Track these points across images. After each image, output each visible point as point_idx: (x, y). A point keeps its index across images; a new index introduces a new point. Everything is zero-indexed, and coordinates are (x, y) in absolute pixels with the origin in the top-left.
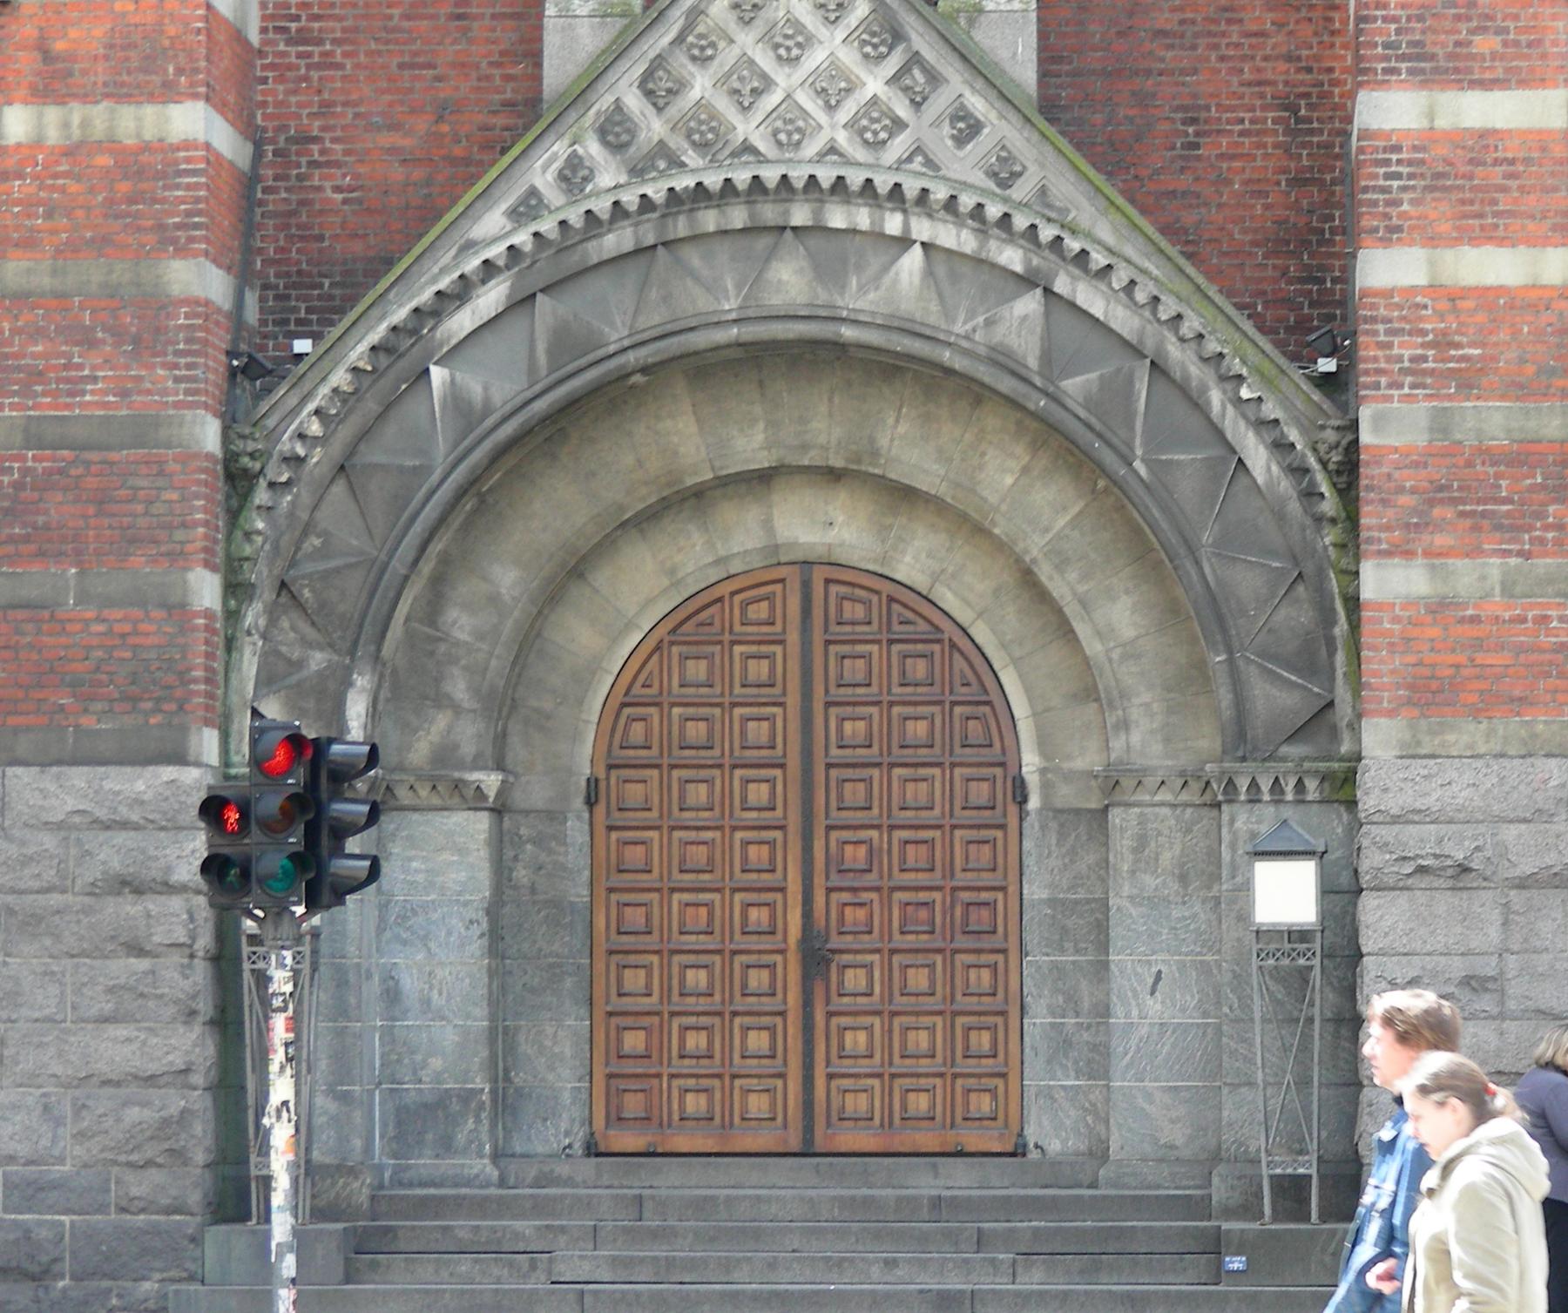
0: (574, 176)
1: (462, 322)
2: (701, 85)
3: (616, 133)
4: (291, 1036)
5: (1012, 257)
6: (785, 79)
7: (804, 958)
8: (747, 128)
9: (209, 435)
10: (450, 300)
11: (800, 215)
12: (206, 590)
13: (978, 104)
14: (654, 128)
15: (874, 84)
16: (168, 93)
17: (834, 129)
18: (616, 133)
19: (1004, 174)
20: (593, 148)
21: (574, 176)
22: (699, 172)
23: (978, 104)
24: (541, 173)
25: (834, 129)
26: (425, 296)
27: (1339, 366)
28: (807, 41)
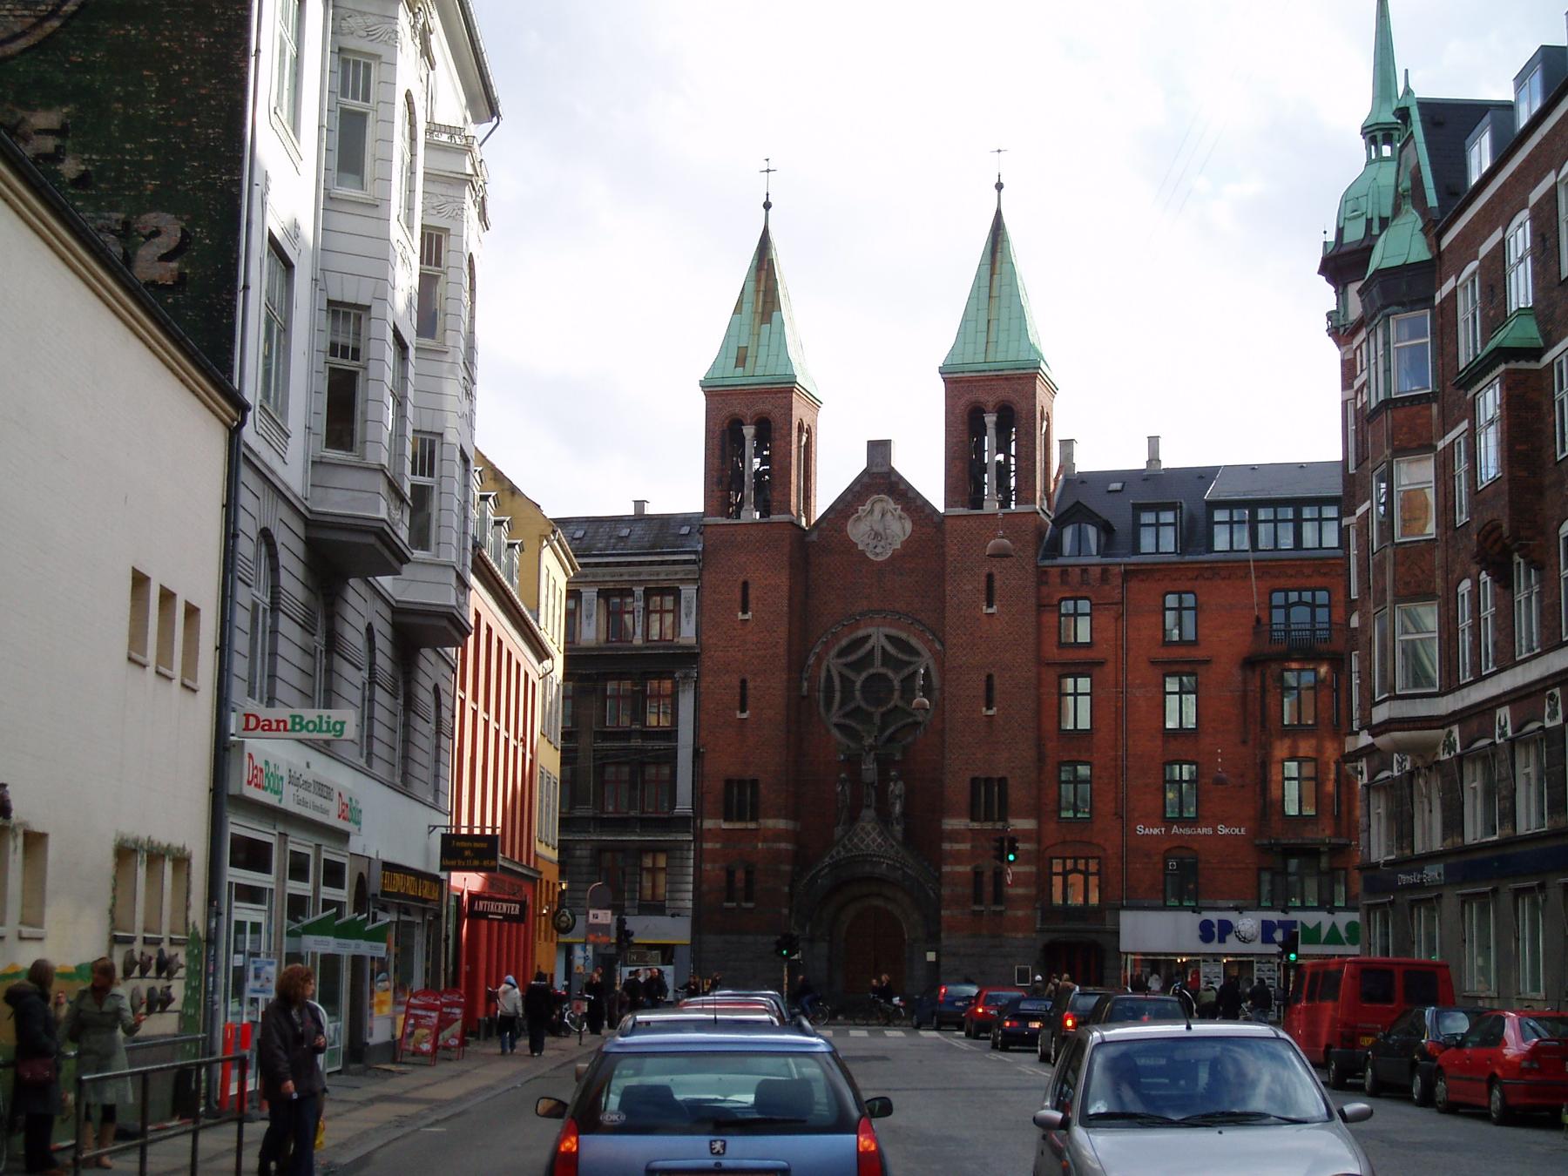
0: (838, 853)
1: (823, 873)
2: (855, 840)
3: (844, 847)
4: (566, 983)
5: (898, 865)
6: (867, 839)
7: (1509, 457)
8: (862, 846)
9: (786, 889)
10: (820, 871)
11: (869, 859)
12: (785, 911)
13: (894, 843)
14: (849, 846)
15: (879, 840)
16: (780, 842)
17: (874, 847)
18: (844, 847)
19: (897, 853)
20: (841, 849)
21: (838, 853)
22: (855, 852)
23: (894, 843)
24: (834, 852)
25: (874, 847)
26: (818, 868)
27: (972, 847)
28: (870, 834)
